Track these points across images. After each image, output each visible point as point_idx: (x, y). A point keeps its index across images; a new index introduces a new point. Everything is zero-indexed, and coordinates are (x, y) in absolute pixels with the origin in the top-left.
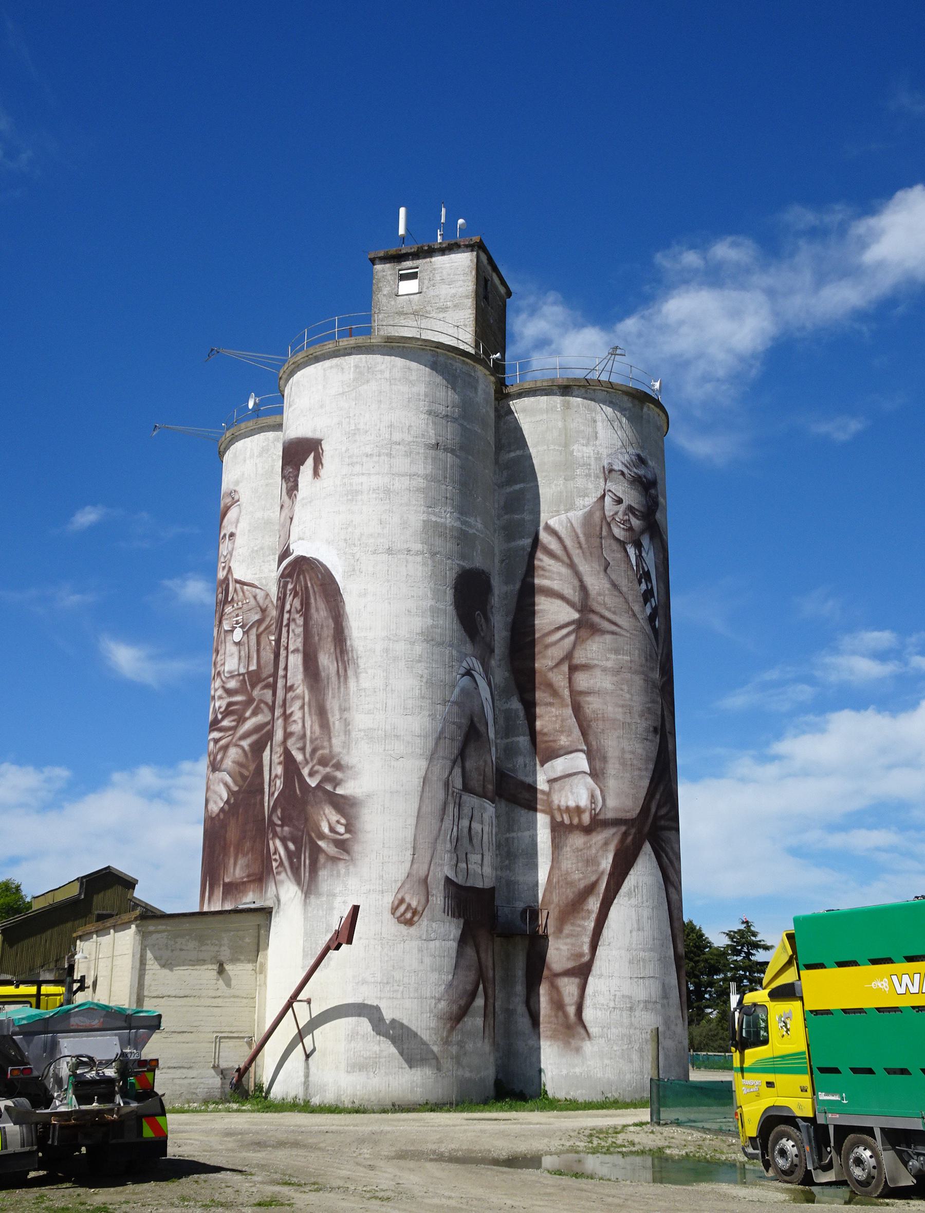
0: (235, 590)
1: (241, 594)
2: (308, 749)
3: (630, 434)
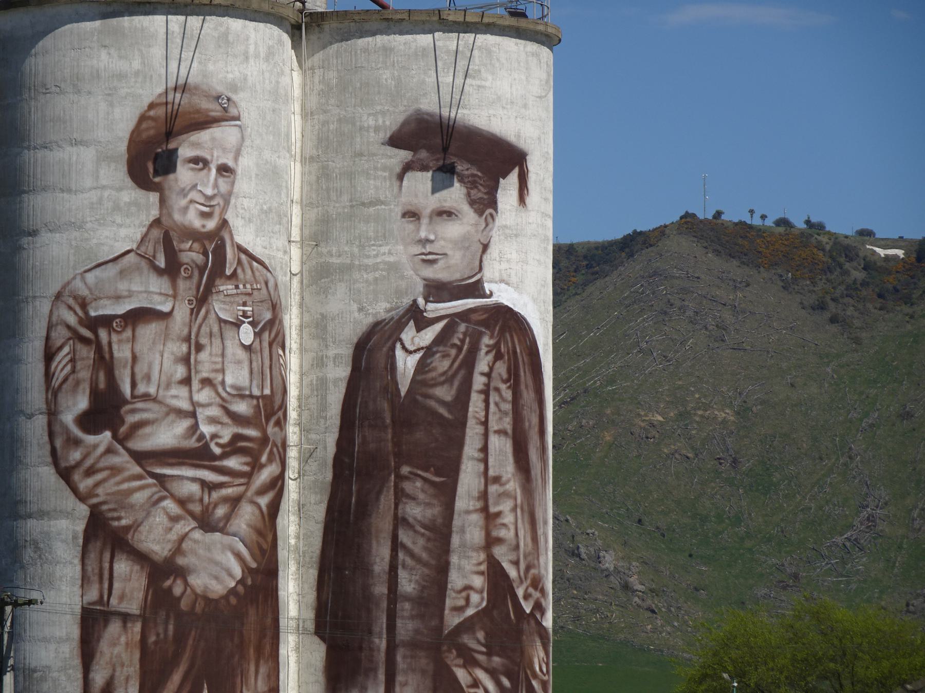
0: (240, 262)
1: (249, 272)
2: (522, 566)
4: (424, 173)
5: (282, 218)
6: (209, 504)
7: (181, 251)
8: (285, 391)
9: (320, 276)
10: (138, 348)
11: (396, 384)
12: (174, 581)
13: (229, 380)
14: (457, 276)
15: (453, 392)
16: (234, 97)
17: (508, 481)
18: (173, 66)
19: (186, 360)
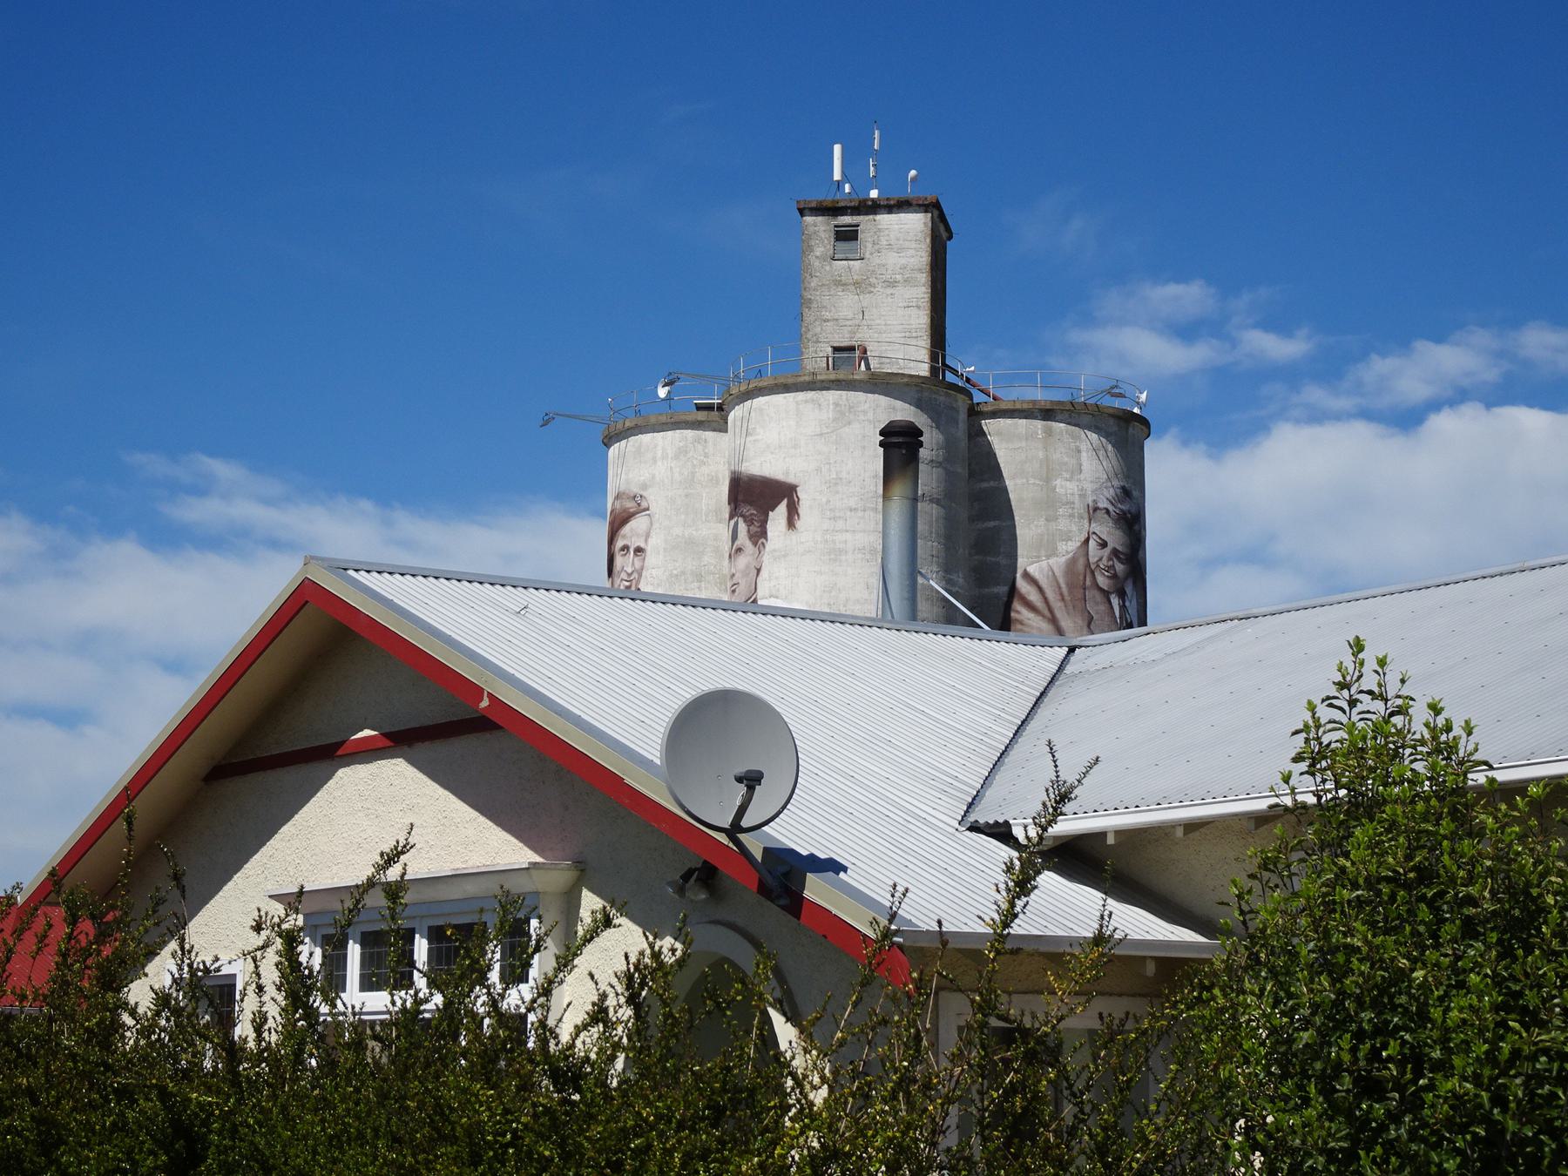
3: (1114, 462)
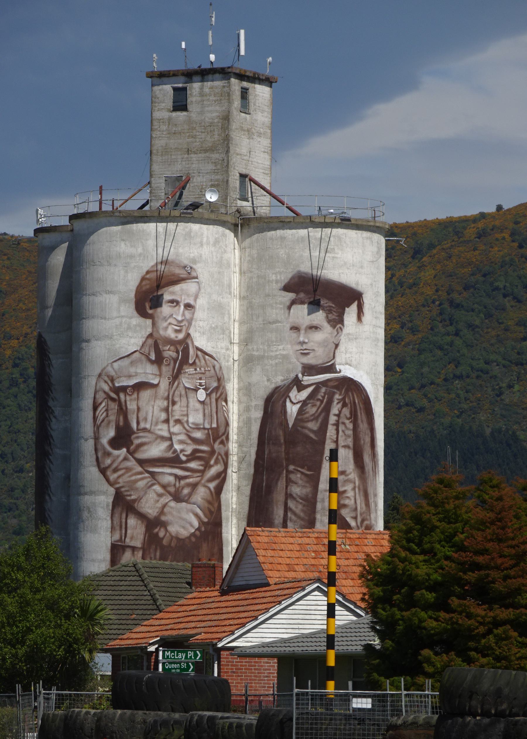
0: (197, 356)
1: (203, 361)
4: (302, 306)
5: (224, 330)
6: (179, 487)
7: (164, 351)
8: (227, 424)
9: (248, 361)
10: (140, 404)
11: (287, 420)
12: (160, 529)
13: (191, 420)
14: (320, 362)
15: (318, 425)
16: (194, 266)
17: (351, 473)
18: (160, 251)
19: (166, 410)
